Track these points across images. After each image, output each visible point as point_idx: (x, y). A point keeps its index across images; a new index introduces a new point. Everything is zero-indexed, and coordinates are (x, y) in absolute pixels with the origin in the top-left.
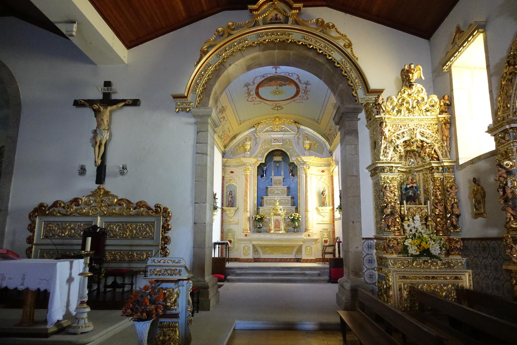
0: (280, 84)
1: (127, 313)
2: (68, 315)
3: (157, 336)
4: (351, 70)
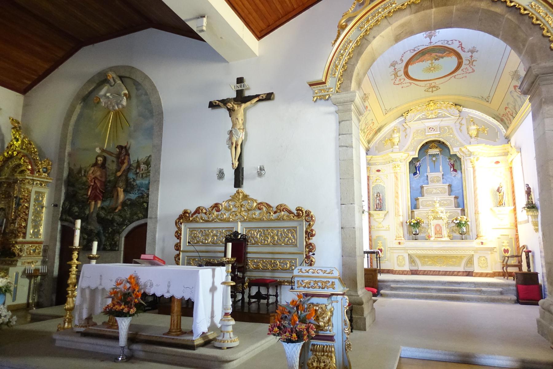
0: (436, 57)
1: (274, 332)
2: (212, 327)
3: (310, 362)
4: (547, 15)
